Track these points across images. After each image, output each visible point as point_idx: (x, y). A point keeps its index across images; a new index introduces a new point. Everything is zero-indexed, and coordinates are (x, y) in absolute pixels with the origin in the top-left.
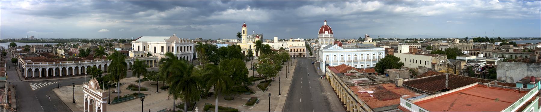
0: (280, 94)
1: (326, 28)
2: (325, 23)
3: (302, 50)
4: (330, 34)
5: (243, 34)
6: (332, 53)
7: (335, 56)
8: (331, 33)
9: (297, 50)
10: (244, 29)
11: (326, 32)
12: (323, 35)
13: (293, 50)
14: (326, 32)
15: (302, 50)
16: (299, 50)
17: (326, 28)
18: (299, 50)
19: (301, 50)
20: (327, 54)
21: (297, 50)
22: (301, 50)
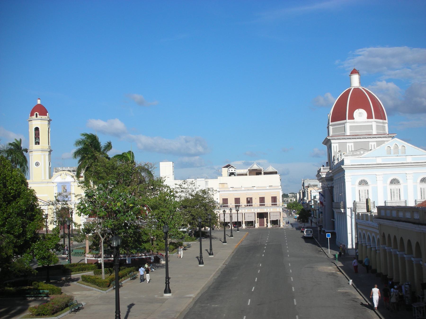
0: (167, 290)
1: (360, 100)
2: (355, 81)
3: (268, 201)
4: (374, 122)
5: (32, 146)
6: (379, 172)
7: (394, 181)
8: (380, 115)
9: (249, 201)
10: (39, 122)
11: (360, 114)
12: (349, 123)
13: (231, 203)
14: (360, 114)
15: (268, 201)
16: (256, 202)
17: (360, 100)
18: (256, 202)
19: (262, 200)
20: (362, 174)
21: (249, 201)
22: (262, 200)
